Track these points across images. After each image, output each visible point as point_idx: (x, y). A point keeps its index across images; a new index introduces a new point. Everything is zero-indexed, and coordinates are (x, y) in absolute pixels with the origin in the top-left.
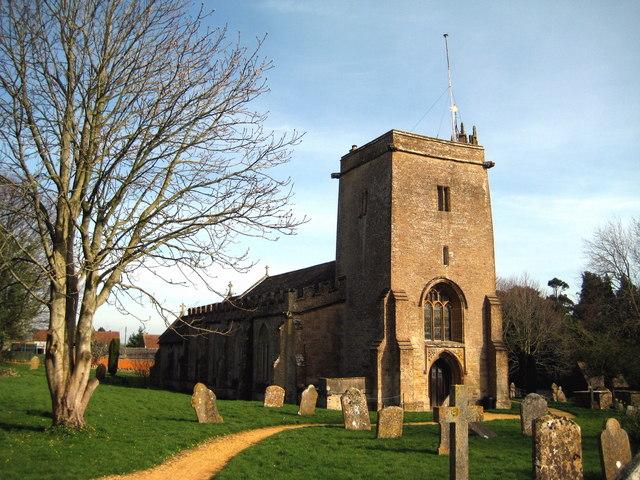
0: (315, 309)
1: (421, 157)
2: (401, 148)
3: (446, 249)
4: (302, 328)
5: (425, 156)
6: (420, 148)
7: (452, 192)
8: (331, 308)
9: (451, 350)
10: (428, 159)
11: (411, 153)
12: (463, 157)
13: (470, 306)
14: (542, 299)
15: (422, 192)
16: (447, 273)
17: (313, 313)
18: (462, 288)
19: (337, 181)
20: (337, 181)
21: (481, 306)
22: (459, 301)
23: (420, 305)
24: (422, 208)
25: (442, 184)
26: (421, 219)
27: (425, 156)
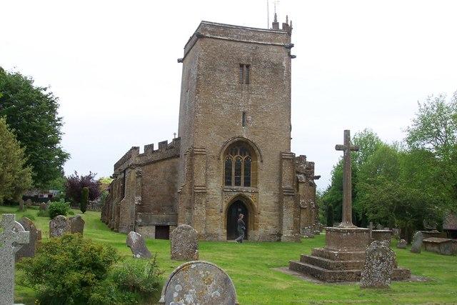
0: (154, 162)
1: (227, 43)
2: (208, 35)
3: (244, 113)
4: (141, 176)
5: (230, 40)
6: (227, 35)
7: (253, 69)
8: (167, 161)
9: (246, 194)
10: (232, 43)
11: (217, 38)
12: (266, 40)
13: (266, 161)
14: (31, 87)
15: (225, 69)
16: (244, 133)
17: (152, 165)
18: (258, 145)
19: (316, 174)
20: (316, 174)
21: (307, 282)
22: (256, 156)
23: (219, 159)
24: (224, 82)
25: (244, 62)
26: (224, 91)
27: (230, 40)
